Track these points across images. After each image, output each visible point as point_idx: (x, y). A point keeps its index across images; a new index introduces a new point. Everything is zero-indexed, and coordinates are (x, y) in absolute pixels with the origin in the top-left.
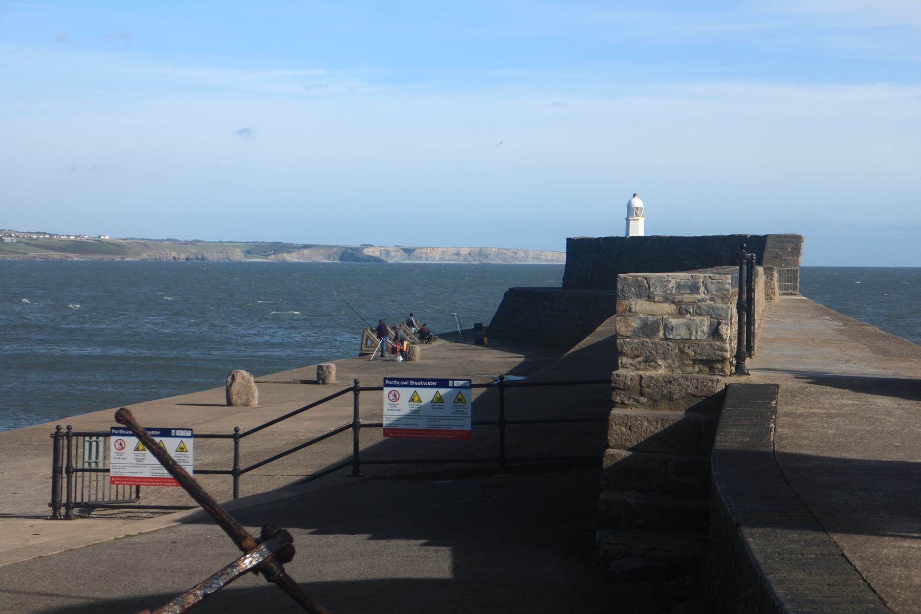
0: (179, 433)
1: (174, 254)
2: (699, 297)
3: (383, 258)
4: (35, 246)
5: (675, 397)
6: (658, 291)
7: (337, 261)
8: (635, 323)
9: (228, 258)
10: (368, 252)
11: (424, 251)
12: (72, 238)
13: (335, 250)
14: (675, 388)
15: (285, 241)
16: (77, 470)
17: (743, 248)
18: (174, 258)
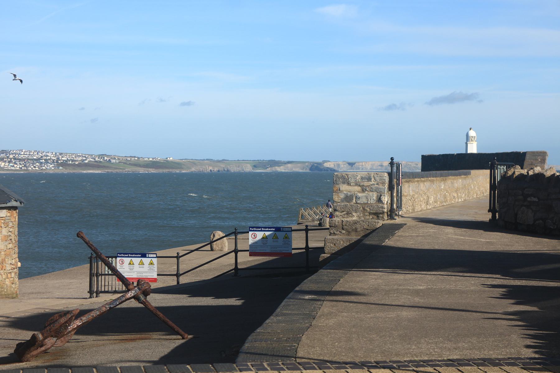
0: (150, 256)
1: (211, 168)
2: (371, 183)
3: (336, 168)
4: (130, 164)
5: (358, 230)
6: (352, 181)
7: (308, 171)
8: (342, 196)
9: (243, 170)
10: (327, 165)
11: (361, 164)
12: (151, 159)
13: (307, 164)
14: (358, 226)
15: (277, 159)
16: (102, 275)
17: (494, 159)
18: (211, 170)
